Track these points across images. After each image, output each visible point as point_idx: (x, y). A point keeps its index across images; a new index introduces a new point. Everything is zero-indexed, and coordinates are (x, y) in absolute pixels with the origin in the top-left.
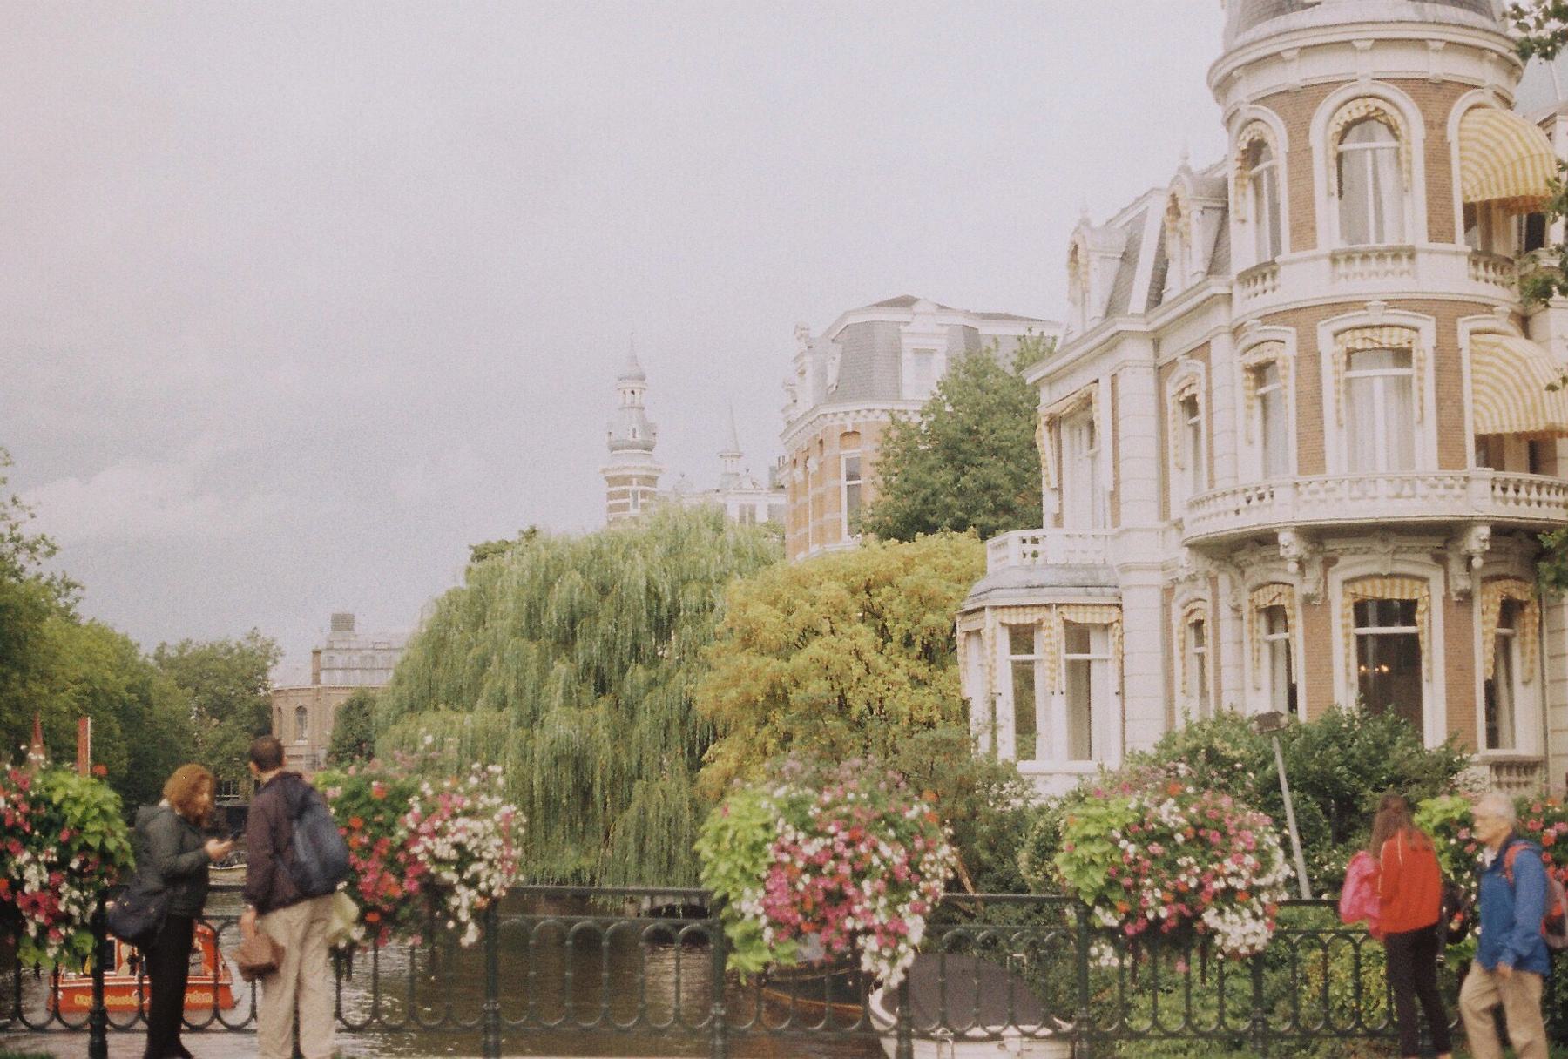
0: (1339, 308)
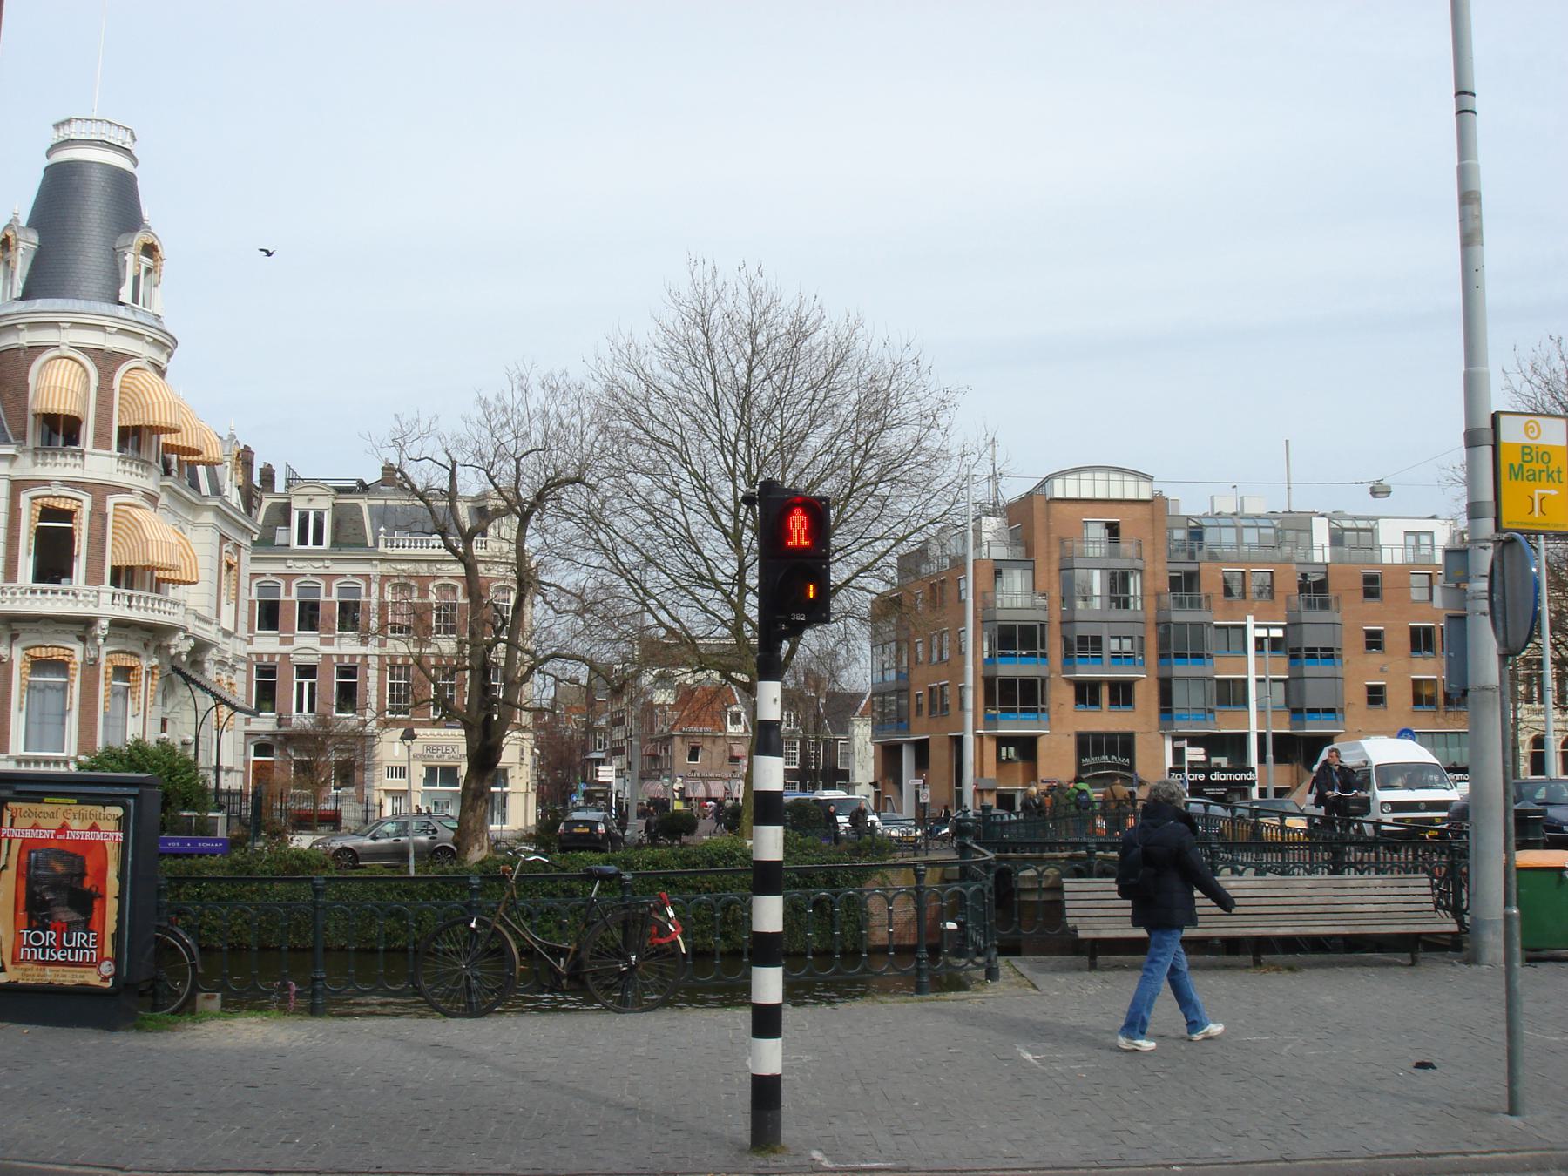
0: (119, 490)
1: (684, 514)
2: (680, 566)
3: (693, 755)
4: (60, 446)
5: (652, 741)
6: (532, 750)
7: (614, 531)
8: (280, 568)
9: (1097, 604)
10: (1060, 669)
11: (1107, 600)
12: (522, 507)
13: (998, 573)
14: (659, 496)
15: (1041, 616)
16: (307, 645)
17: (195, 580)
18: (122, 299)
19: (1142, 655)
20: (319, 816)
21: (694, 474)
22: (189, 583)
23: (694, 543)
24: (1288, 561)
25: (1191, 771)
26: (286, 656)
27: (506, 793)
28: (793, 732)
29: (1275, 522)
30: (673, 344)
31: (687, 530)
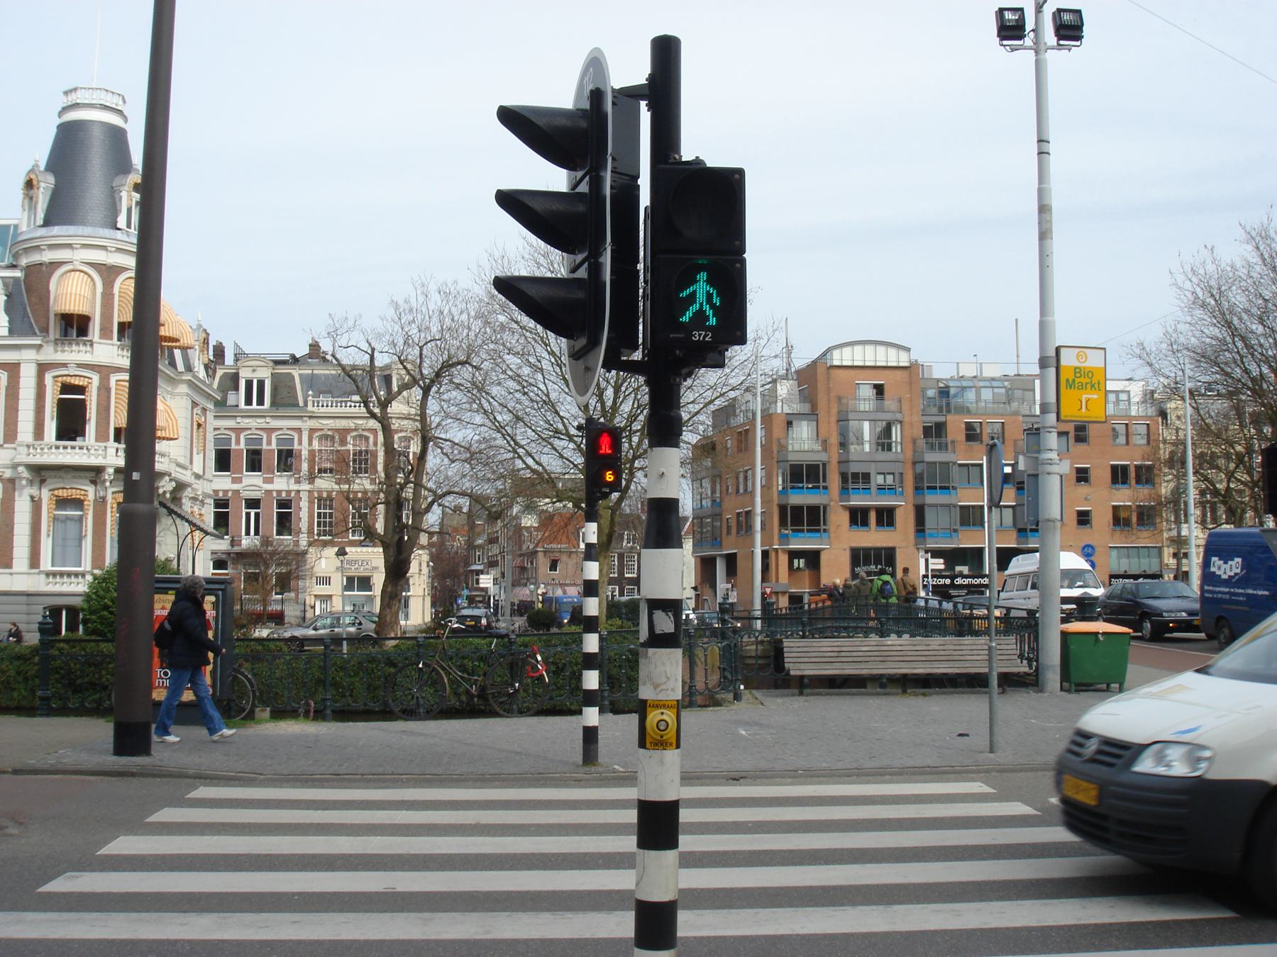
1: (545, 383)
2: (542, 423)
3: (553, 566)
4: (75, 337)
5: (521, 555)
6: (428, 563)
7: (493, 398)
8: (231, 423)
9: (867, 448)
10: (838, 499)
11: (874, 446)
12: (424, 383)
13: (789, 424)
14: (526, 371)
15: (823, 457)
16: (253, 484)
17: (176, 437)
18: (118, 226)
19: (902, 487)
20: (268, 614)
21: (552, 353)
22: (171, 439)
23: (553, 406)
24: (1016, 413)
25: (933, 577)
26: (237, 492)
27: (409, 597)
28: (632, 548)
29: (1006, 383)
30: (536, 255)
31: (547, 395)
